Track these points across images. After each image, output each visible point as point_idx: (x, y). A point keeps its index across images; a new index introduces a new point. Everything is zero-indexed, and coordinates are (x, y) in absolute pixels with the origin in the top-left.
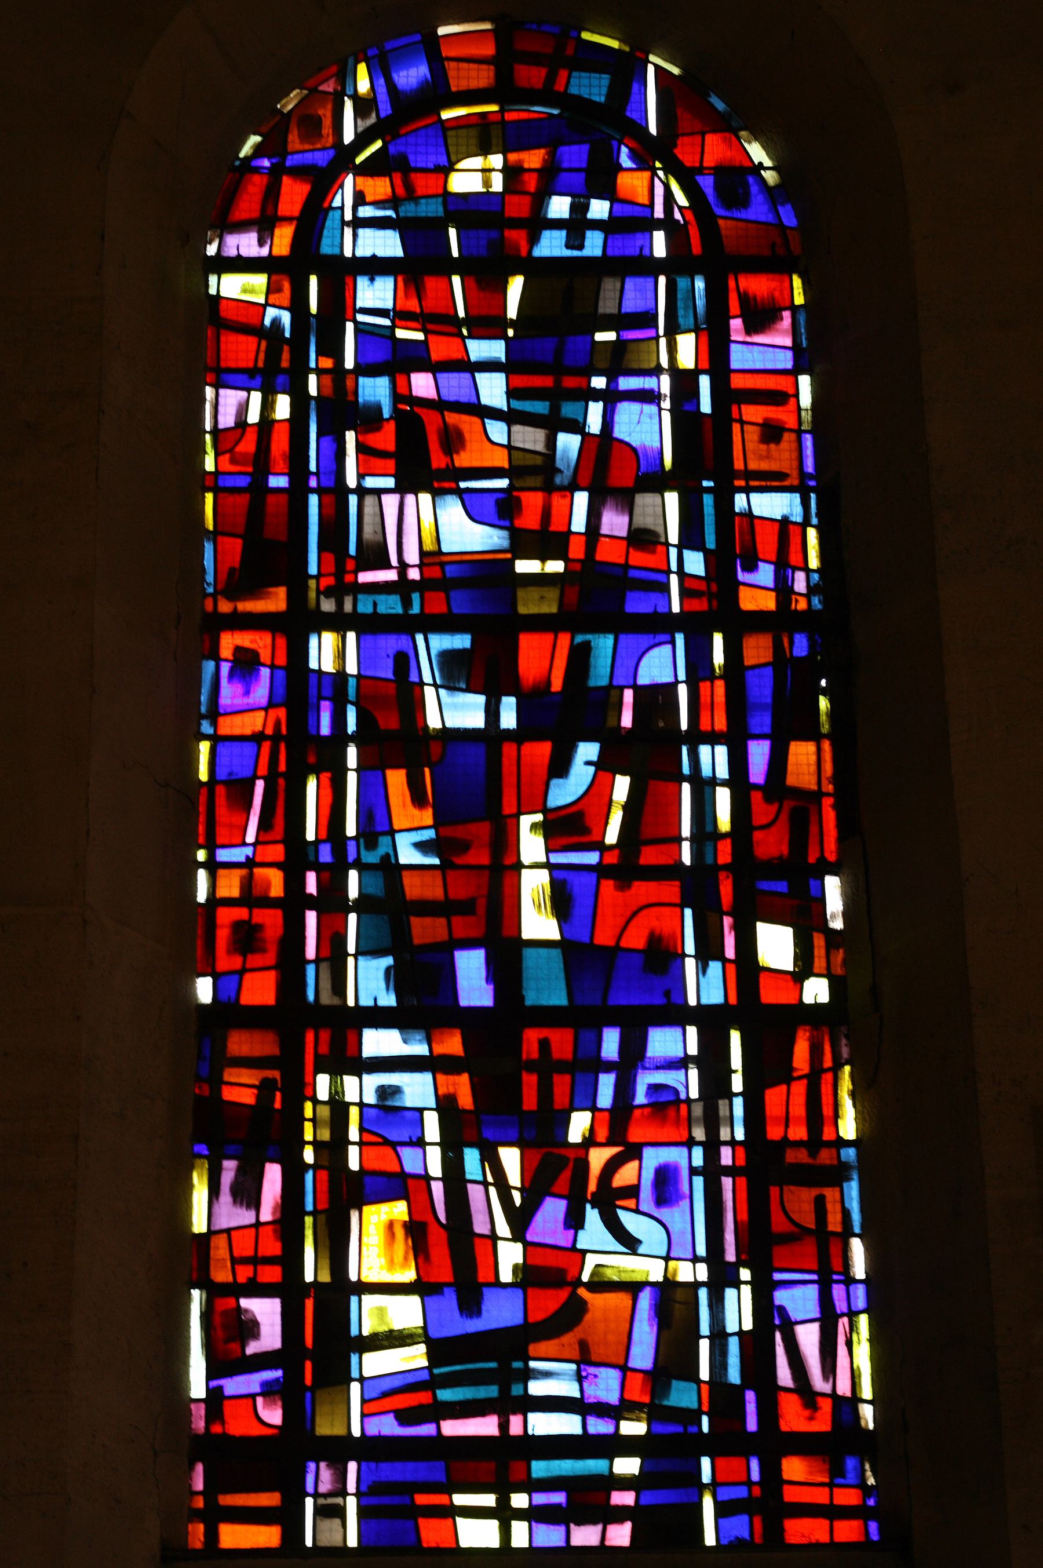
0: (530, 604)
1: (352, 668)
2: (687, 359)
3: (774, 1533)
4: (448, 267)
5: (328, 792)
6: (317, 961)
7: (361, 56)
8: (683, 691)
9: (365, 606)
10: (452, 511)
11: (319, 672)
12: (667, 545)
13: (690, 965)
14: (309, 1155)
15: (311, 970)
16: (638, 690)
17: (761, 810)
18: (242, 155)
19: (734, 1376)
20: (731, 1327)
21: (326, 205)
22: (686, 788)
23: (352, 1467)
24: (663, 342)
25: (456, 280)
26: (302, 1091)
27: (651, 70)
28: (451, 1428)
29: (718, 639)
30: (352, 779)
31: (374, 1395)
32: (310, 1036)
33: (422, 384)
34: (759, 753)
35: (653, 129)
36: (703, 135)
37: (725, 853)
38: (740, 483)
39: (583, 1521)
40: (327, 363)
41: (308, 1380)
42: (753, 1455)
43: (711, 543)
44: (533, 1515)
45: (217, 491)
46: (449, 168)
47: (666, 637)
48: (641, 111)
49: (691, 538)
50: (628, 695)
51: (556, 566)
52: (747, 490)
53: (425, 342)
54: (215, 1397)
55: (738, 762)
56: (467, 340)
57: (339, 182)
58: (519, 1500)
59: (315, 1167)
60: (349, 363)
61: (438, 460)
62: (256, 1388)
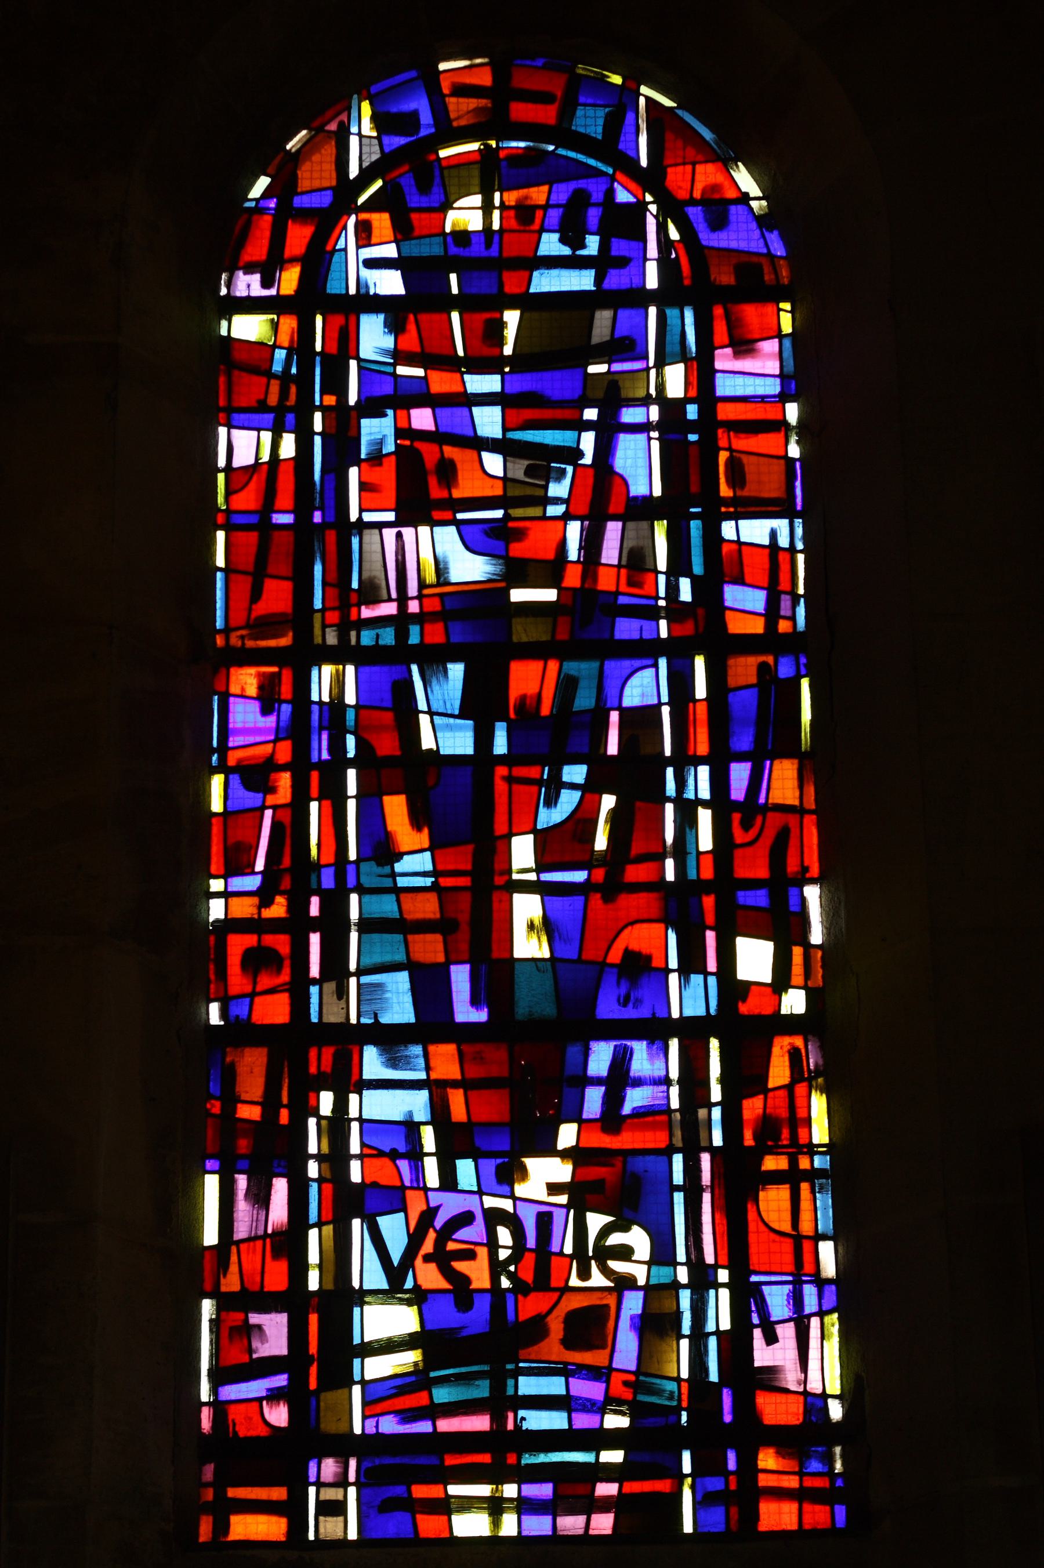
0: (523, 632)
1: (350, 698)
5: (328, 820)
7: (364, 92)
8: (666, 710)
9: (367, 638)
10: (448, 537)
12: (657, 572)
14: (313, 1169)
21: (329, 248)
22: (669, 808)
24: (653, 373)
25: (455, 316)
27: (642, 101)
28: (445, 1425)
29: (700, 662)
30: (352, 805)
32: (313, 1053)
33: (422, 419)
34: (740, 774)
35: (644, 162)
40: (330, 400)
41: (313, 1385)
43: (698, 569)
44: (524, 1506)
46: (447, 205)
47: (650, 662)
49: (679, 565)
50: (614, 716)
52: (736, 517)
55: (720, 782)
57: (342, 223)
58: (510, 1490)
59: (320, 1180)
60: (353, 398)
61: (436, 492)
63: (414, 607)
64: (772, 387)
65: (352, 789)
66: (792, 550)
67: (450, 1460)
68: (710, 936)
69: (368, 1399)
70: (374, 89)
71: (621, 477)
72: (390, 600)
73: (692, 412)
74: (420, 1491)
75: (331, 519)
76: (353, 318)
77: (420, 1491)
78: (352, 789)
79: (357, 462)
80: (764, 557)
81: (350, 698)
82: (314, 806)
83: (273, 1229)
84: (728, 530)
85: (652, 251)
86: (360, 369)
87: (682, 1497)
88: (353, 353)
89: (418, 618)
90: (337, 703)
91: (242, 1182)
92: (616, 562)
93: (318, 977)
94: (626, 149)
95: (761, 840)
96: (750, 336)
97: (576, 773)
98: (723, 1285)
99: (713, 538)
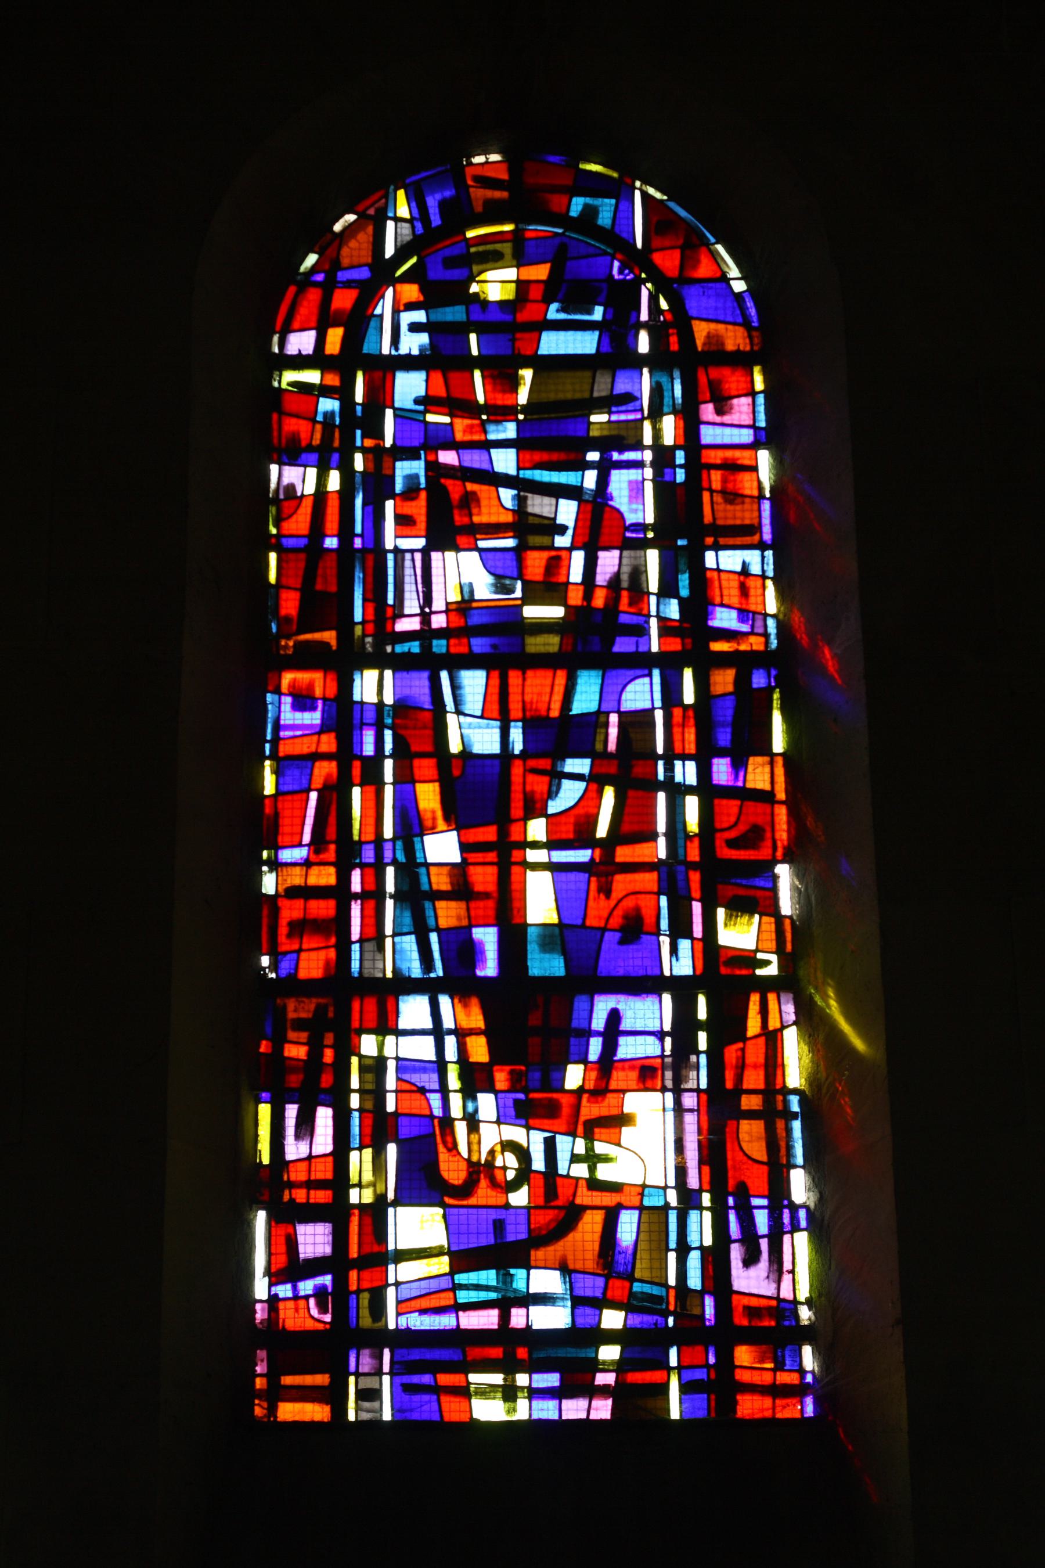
0: (536, 644)
2: (669, 439)
6: (361, 941)
8: (659, 715)
11: (362, 703)
13: (665, 942)
14: (355, 1101)
15: (356, 947)
19: (694, 1281)
22: (661, 797)
23: (387, 1354)
26: (347, 1048)
30: (389, 792)
33: (448, 457)
35: (639, 244)
37: (694, 854)
38: (709, 540)
39: (572, 1395)
40: (369, 443)
43: (684, 592)
44: (535, 1393)
47: (646, 672)
48: (628, 225)
49: (668, 589)
50: (614, 718)
51: (557, 612)
52: (717, 548)
53: (451, 424)
54: (273, 1301)
55: (704, 772)
58: (522, 1379)
60: (388, 442)
61: (459, 519)
63: (439, 621)
64: (746, 436)
66: (763, 577)
68: (697, 907)
73: (680, 457)
74: (444, 1379)
75: (370, 545)
76: (389, 376)
79: (392, 495)
82: (356, 792)
83: (641, 374)
86: (396, 416)
88: (388, 403)
91: (291, 1111)
96: (726, 394)
97: (580, 765)
98: (707, 1209)
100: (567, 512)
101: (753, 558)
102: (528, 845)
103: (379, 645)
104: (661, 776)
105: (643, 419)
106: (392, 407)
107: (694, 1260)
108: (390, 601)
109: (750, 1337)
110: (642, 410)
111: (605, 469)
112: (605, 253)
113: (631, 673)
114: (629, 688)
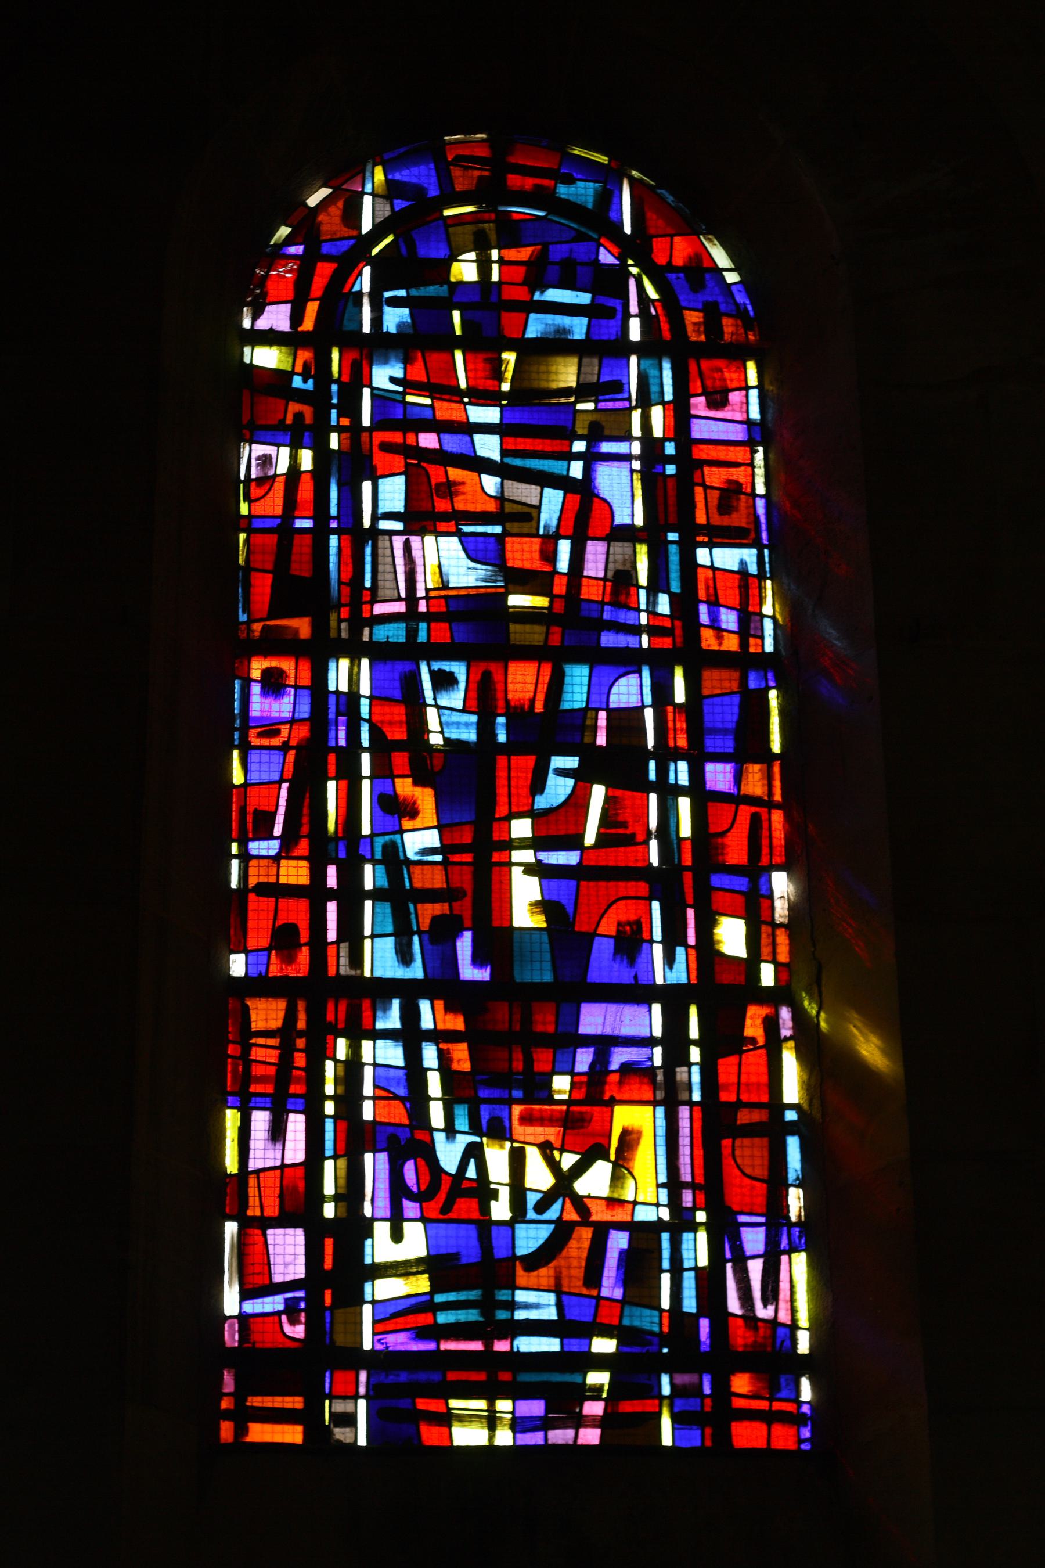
2: (658, 432)
3: (723, 1436)
4: (452, 343)
8: (649, 714)
10: (451, 545)
14: (329, 1108)
16: (610, 712)
17: (719, 815)
18: (468, 935)
19: (690, 1305)
20: (688, 1264)
22: (653, 798)
25: (459, 355)
31: (382, 1316)
32: (330, 1006)
35: (628, 229)
36: (672, 236)
40: (345, 422)
42: (707, 1372)
43: (675, 587)
45: (249, 531)
49: (657, 584)
52: (711, 545)
55: (697, 774)
56: (468, 407)
58: (504, 1406)
60: (366, 421)
62: (281, 1307)
64: (737, 433)
65: (366, 769)
67: (452, 1376)
69: (377, 1318)
70: (386, 156)
71: (605, 500)
72: (399, 599)
73: (670, 449)
77: (422, 1404)
78: (366, 769)
80: (736, 581)
81: (365, 689)
82: (332, 785)
84: (702, 556)
85: (634, 308)
86: (373, 396)
87: (631, 215)
88: (365, 382)
89: (427, 617)
90: (353, 696)
92: (601, 574)
93: (336, 887)
94: (619, 685)
95: (734, 830)
99: (689, 564)
100: (552, 503)
101: (749, 555)
102: (512, 845)
103: (356, 630)
104: (652, 776)
105: (631, 409)
106: (370, 386)
107: (689, 1281)
108: (368, 584)
109: (744, 1362)
110: (629, 399)
111: (591, 458)
112: (591, 239)
113: (622, 670)
114: (615, 690)
